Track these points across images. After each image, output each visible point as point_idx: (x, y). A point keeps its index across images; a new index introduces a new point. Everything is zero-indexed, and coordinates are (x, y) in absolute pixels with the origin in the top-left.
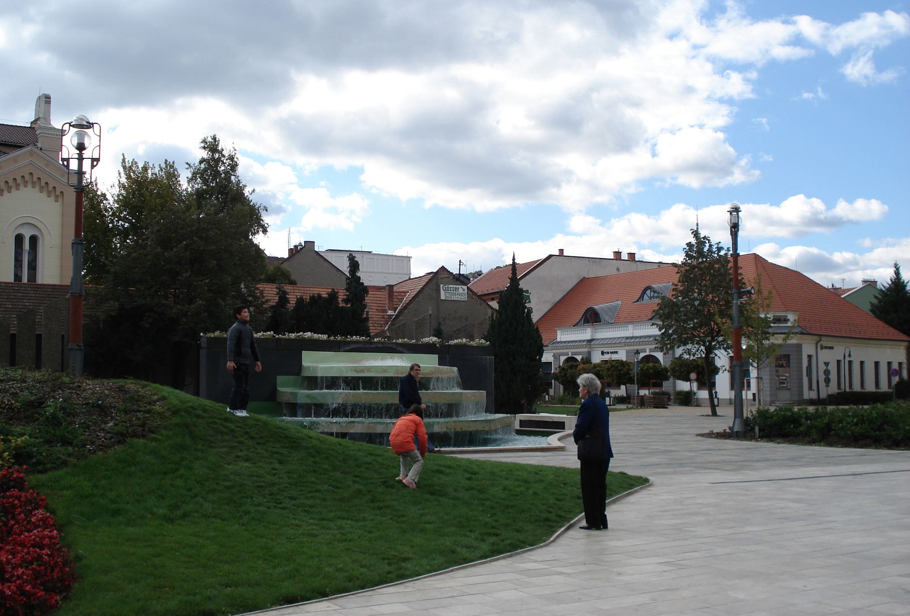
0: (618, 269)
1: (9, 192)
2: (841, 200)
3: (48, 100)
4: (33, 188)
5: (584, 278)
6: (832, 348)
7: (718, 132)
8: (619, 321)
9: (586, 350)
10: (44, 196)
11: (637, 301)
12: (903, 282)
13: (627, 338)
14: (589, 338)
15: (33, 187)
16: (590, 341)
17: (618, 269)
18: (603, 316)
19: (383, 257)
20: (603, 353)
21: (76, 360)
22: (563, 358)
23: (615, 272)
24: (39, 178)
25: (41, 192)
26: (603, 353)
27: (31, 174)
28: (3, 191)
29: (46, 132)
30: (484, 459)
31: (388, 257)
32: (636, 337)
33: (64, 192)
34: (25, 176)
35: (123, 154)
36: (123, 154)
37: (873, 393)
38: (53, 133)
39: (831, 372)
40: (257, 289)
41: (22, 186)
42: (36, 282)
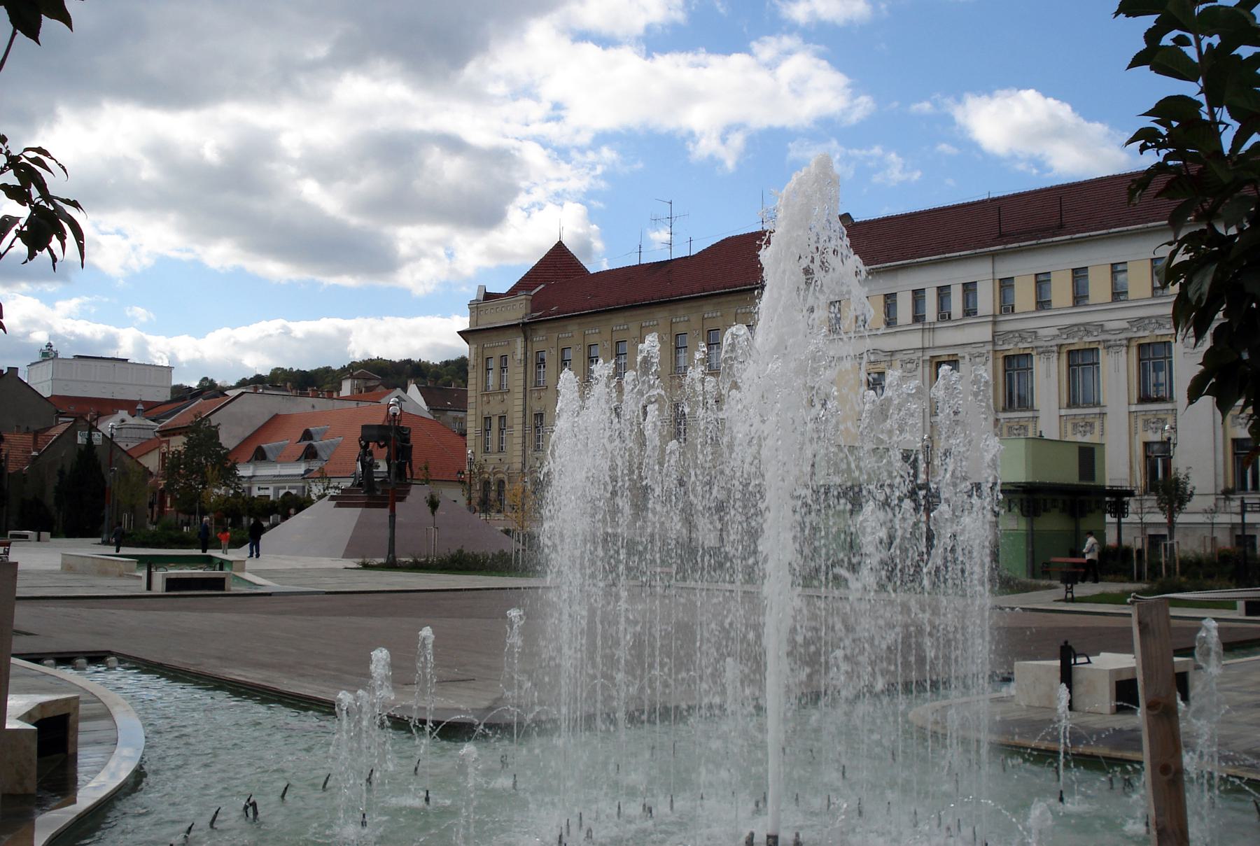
0: (313, 407)
5: (277, 415)
8: (282, 460)
9: (301, 484)
11: (299, 442)
12: (1177, 479)
13: (275, 476)
14: (251, 475)
16: (250, 477)
17: (313, 407)
18: (270, 455)
19: (138, 367)
20: (259, 489)
21: (227, 547)
22: (282, 492)
23: (310, 410)
26: (259, 489)
30: (282, 556)
31: (144, 367)
32: (283, 476)
37: (1077, 485)
42: (1093, 479)
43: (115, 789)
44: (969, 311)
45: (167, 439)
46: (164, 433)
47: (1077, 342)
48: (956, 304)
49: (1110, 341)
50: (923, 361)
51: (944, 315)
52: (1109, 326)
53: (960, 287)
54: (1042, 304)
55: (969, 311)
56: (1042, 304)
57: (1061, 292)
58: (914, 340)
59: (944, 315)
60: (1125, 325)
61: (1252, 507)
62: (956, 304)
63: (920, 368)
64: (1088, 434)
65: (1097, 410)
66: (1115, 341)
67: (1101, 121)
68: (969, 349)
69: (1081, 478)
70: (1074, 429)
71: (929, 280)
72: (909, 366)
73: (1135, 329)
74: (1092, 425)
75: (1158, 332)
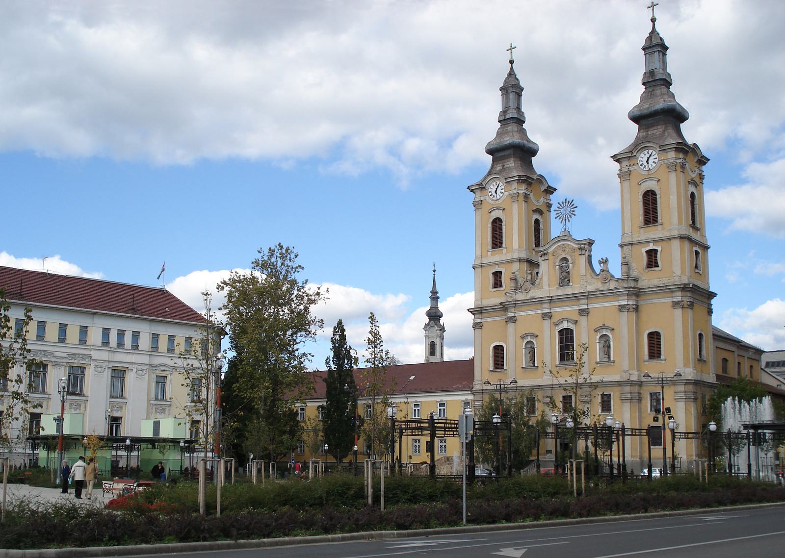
43: (708, 268)
44: (135, 347)
45: (623, 277)
46: (431, 318)
47: (76, 362)
48: (128, 341)
49: (57, 362)
50: (108, 368)
51: (120, 345)
52: (57, 354)
53: (116, 332)
54: (62, 339)
55: (135, 347)
56: (62, 339)
57: (73, 335)
58: (145, 359)
59: (120, 345)
60: (65, 355)
61: (640, 432)
62: (128, 341)
63: (147, 375)
64: (119, 412)
65: (84, 398)
66: (60, 362)
67: (78, 266)
68: (136, 366)
69: (153, 436)
70: (70, 406)
71: (115, 325)
72: (99, 369)
73: (70, 359)
74: (80, 405)
75: (81, 362)
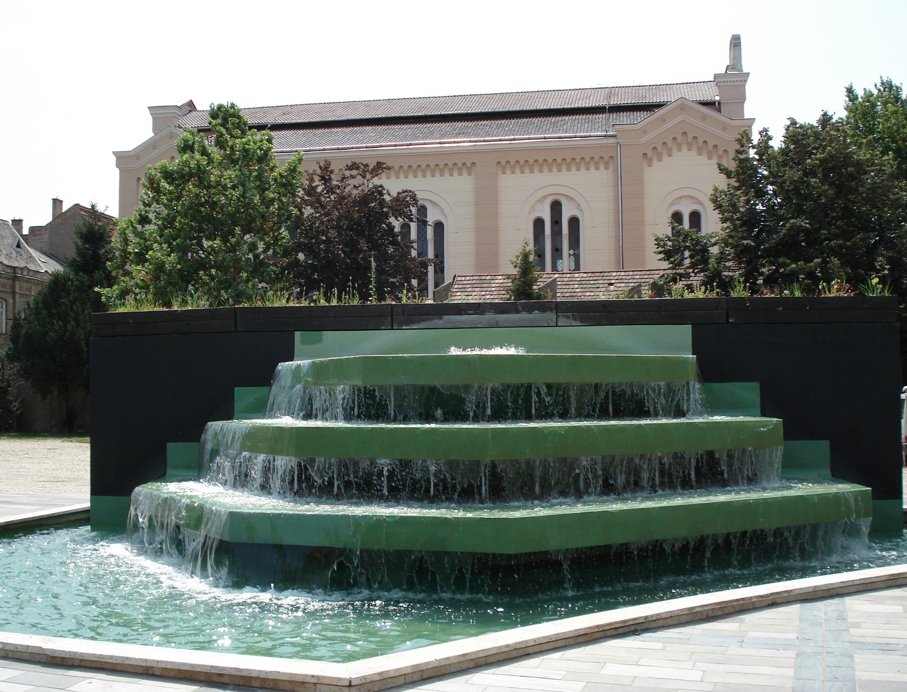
1: (660, 160)
2: (88, 439)
3: (736, 42)
4: (689, 150)
6: (439, 227)
7: (96, 626)
10: (704, 158)
15: (690, 149)
24: (705, 141)
25: (699, 155)
27: (685, 133)
28: (652, 160)
29: (727, 80)
33: (728, 150)
34: (677, 138)
35: (736, 42)
36: (736, 42)
38: (732, 79)
39: (568, 216)
40: (528, 280)
41: (675, 151)
